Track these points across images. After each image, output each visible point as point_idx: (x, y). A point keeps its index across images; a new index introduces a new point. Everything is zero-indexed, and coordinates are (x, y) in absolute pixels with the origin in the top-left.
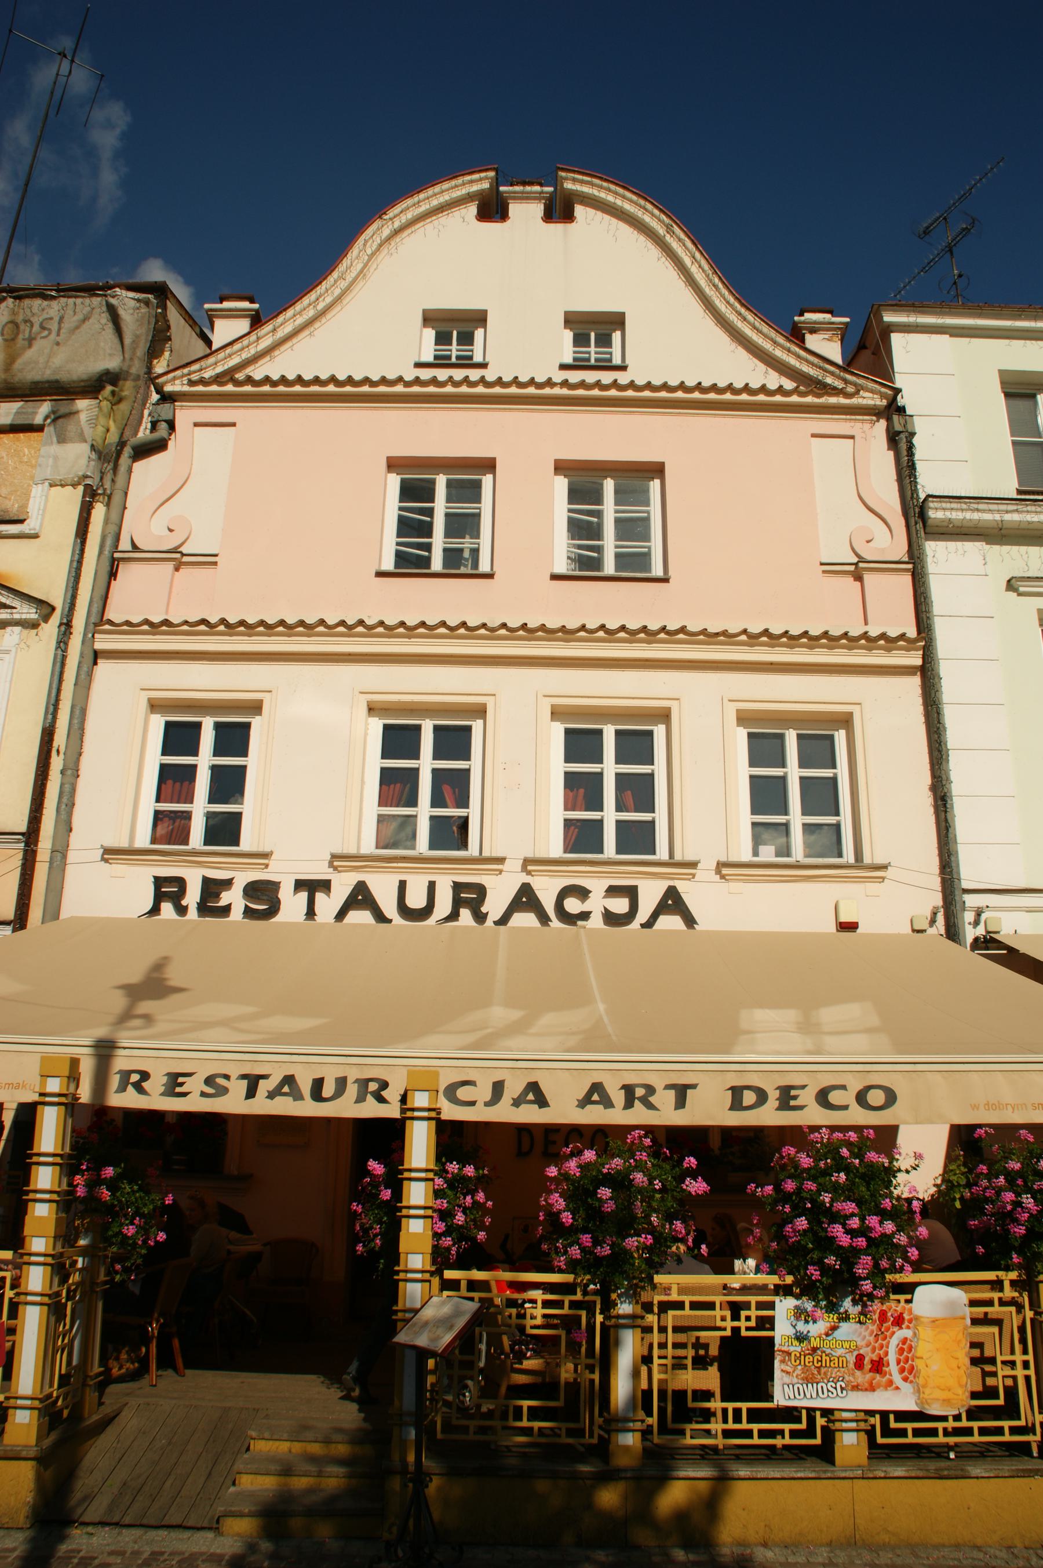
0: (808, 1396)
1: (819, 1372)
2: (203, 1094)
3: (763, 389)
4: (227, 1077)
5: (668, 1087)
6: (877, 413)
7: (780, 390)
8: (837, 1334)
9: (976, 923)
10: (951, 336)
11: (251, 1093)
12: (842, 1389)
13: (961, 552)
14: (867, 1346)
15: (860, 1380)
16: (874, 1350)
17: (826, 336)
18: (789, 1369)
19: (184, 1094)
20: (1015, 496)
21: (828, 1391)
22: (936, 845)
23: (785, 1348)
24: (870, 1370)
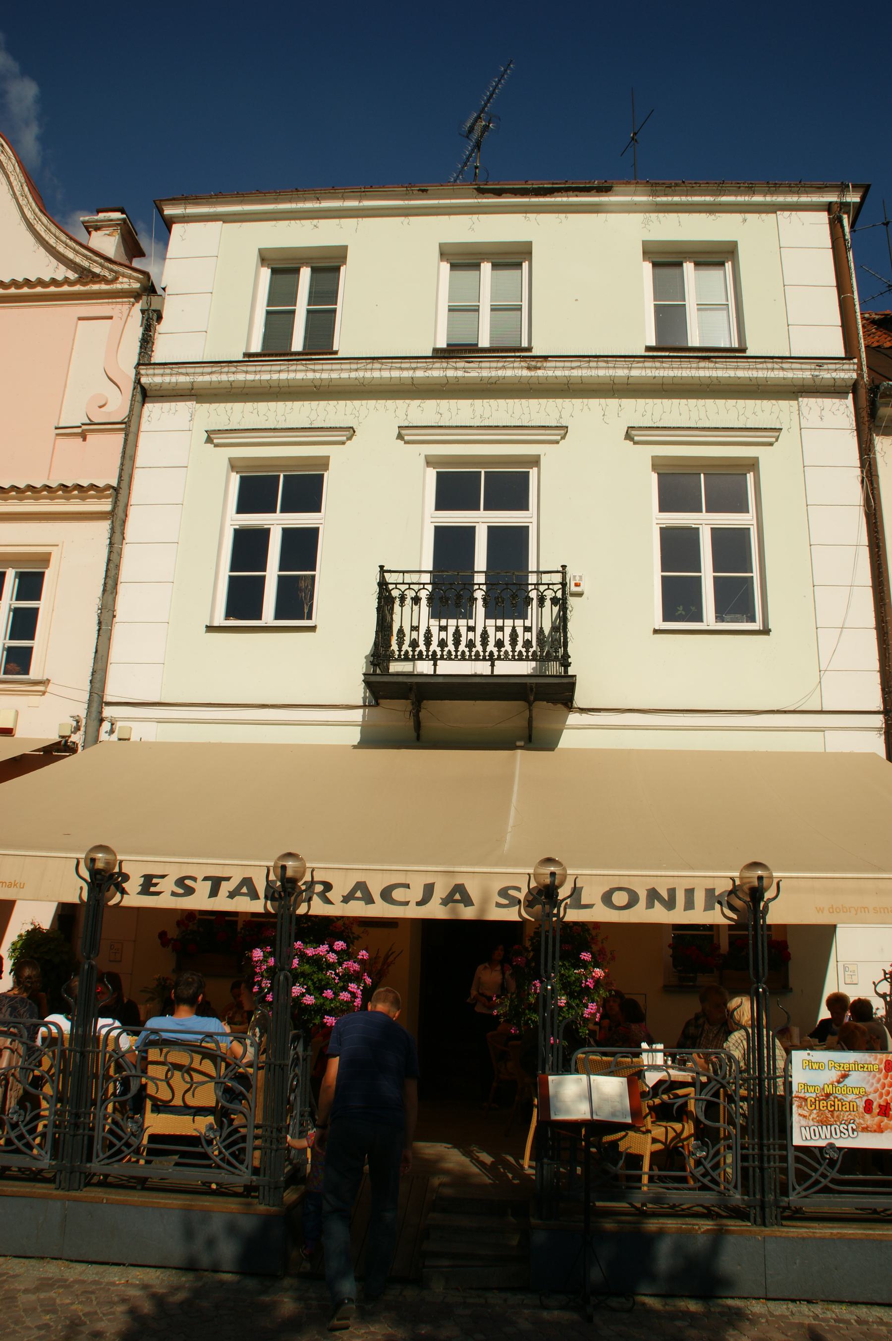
0: (823, 1137)
1: (832, 1116)
2: (174, 894)
3: (54, 282)
4: (194, 879)
5: (206, 879)
6: (136, 296)
7: (67, 281)
8: (848, 1081)
9: (112, 731)
10: (224, 222)
11: (214, 893)
12: (853, 1130)
13: (173, 411)
14: (875, 1092)
15: (869, 1123)
16: (881, 1096)
17: (107, 232)
18: (805, 1113)
19: (158, 893)
20: (241, 359)
21: (841, 1132)
22: (877, 657)
23: (802, 1095)
24: (879, 1114)
